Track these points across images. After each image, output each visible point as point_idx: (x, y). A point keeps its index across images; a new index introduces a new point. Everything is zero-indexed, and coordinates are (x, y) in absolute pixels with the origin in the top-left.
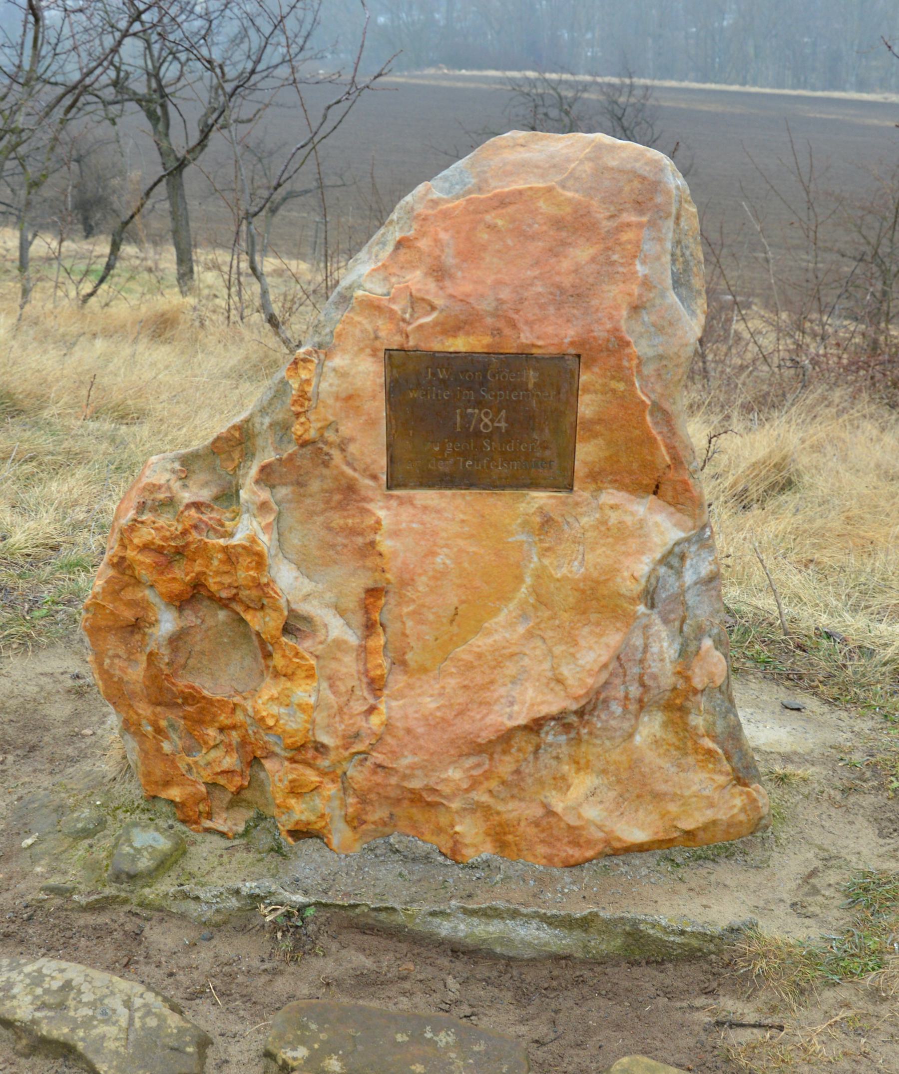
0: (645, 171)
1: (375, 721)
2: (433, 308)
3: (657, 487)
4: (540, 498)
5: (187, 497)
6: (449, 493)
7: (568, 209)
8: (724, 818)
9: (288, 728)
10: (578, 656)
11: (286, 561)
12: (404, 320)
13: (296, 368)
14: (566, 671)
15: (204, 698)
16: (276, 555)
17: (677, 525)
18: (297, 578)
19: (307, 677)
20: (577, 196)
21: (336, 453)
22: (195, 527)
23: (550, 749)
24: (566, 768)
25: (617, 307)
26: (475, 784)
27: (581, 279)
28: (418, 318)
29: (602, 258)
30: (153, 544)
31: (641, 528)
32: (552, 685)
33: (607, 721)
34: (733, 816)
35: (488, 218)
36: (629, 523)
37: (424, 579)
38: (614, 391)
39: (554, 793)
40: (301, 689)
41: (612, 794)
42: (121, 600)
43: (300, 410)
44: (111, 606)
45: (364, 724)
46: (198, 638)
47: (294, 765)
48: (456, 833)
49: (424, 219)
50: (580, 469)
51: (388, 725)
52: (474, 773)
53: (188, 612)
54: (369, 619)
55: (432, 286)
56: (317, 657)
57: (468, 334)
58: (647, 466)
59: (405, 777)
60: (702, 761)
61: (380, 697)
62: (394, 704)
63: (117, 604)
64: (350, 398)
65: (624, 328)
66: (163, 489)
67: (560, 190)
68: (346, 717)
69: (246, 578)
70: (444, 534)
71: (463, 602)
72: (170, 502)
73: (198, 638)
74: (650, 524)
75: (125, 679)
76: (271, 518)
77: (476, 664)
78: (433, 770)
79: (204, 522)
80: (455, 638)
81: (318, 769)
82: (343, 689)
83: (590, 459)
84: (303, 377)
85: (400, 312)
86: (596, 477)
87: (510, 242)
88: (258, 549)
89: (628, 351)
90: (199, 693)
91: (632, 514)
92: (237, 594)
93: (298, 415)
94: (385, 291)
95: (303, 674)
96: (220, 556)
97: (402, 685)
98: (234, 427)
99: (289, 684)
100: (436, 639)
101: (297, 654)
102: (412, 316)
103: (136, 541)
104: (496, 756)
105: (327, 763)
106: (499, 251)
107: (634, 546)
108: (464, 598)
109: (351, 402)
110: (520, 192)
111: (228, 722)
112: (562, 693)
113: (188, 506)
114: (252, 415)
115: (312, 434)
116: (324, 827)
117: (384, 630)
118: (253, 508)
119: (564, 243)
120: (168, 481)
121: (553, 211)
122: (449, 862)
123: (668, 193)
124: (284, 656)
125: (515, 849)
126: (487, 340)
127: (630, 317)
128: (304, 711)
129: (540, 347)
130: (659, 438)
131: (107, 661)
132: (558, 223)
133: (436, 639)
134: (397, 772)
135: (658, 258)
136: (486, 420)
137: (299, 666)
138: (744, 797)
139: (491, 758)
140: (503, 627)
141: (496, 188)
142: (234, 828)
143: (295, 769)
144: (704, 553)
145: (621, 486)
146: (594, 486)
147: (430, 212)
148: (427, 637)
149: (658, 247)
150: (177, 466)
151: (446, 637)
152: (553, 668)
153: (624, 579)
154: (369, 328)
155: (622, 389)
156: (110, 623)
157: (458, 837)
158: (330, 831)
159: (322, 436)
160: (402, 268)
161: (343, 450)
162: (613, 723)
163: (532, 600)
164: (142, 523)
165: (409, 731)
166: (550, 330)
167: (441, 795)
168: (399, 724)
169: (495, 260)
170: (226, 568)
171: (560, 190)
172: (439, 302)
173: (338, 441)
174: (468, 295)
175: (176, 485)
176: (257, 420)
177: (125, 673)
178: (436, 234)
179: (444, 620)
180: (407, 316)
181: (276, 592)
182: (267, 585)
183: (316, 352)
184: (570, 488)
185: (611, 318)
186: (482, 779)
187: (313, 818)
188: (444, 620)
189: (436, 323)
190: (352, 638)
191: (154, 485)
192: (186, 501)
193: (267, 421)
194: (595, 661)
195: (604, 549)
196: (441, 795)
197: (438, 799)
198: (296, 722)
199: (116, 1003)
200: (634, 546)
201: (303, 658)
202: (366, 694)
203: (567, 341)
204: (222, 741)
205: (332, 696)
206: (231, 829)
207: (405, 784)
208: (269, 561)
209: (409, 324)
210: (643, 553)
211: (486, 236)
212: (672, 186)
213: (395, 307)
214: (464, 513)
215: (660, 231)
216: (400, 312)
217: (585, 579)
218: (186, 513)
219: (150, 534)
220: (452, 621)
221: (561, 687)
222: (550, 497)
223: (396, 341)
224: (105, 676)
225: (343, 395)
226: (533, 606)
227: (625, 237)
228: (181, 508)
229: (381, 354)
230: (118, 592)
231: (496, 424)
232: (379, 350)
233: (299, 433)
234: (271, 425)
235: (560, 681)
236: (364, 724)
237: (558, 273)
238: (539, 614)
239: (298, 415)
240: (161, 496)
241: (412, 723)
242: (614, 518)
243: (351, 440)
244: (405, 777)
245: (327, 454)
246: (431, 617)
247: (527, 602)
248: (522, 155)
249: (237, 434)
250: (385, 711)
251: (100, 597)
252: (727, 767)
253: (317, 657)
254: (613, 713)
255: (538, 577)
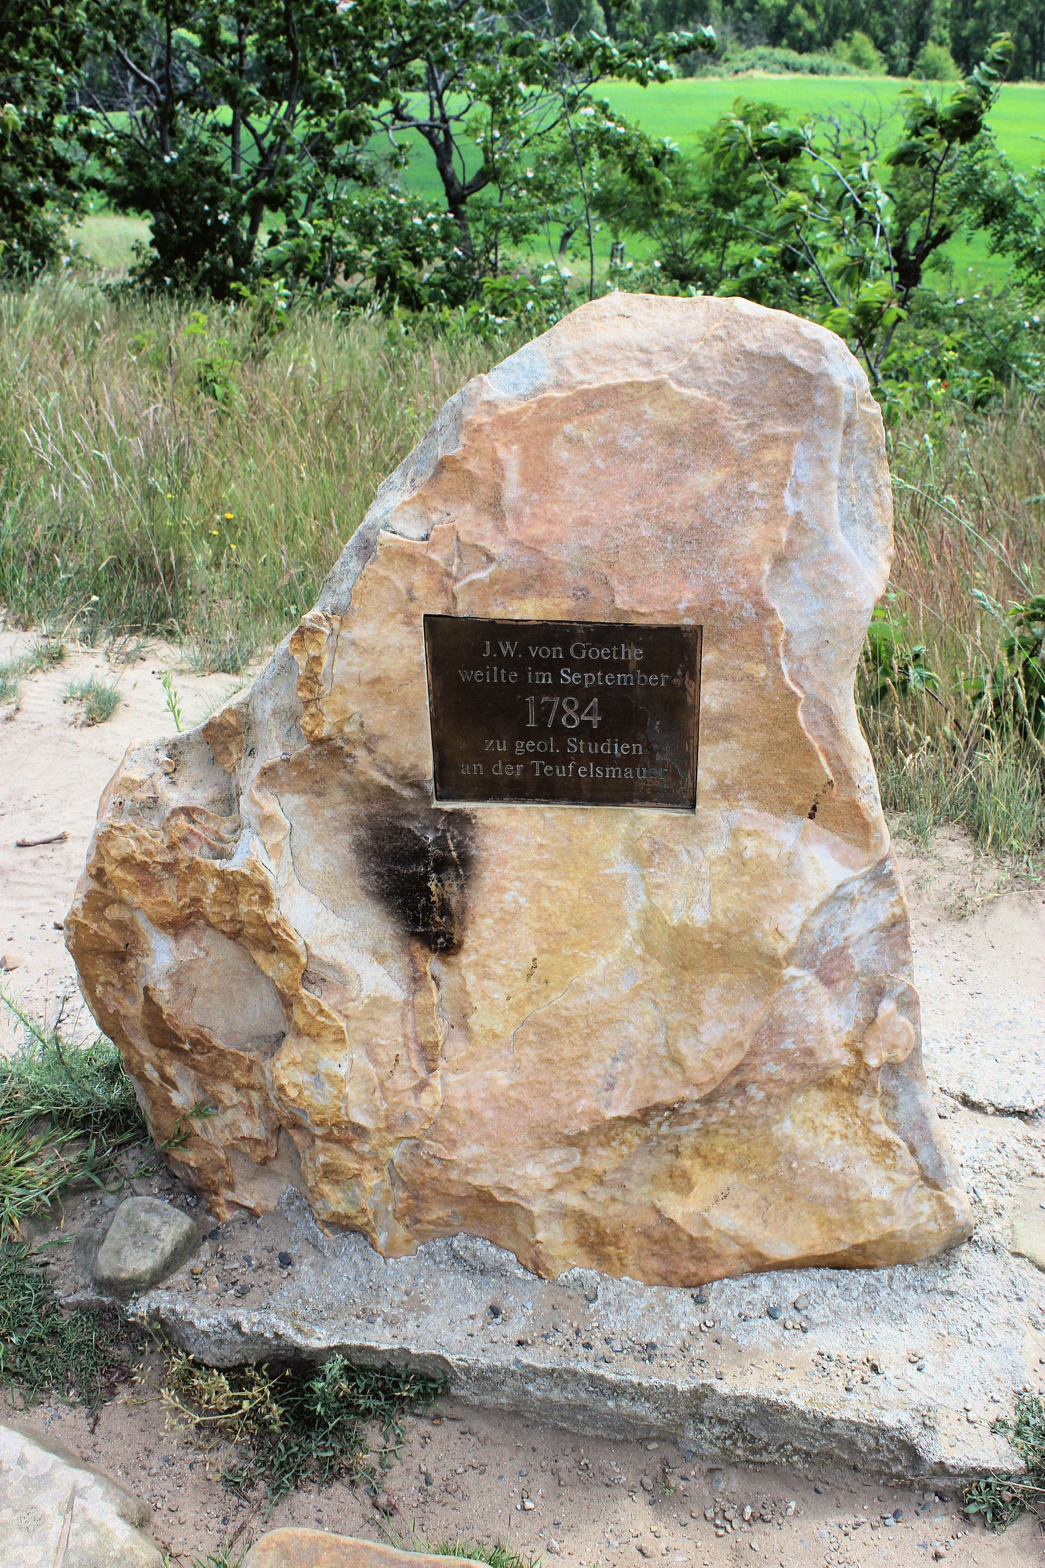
0: (799, 357)
1: (426, 1099)
2: (490, 559)
3: (814, 808)
4: (651, 816)
5: (174, 797)
6: (520, 807)
7: (686, 415)
8: (906, 1228)
9: (315, 1103)
10: (701, 1029)
11: (304, 891)
12: (449, 575)
13: (302, 640)
14: (685, 1048)
15: (214, 1047)
16: (289, 884)
17: (845, 861)
18: (318, 915)
19: (336, 1041)
20: (699, 394)
21: (360, 753)
22: (185, 840)
23: (665, 1142)
24: (688, 1163)
25: (757, 560)
26: (563, 1182)
27: (702, 517)
28: (469, 573)
29: (732, 488)
30: (134, 858)
31: (791, 864)
32: (667, 1064)
33: (744, 1108)
34: (918, 1226)
35: (569, 428)
36: (774, 857)
37: (489, 921)
38: (751, 677)
39: (671, 1194)
40: (328, 1055)
41: (753, 1197)
42: (106, 920)
43: (309, 696)
44: (94, 926)
45: (412, 1103)
46: (205, 972)
47: (328, 1145)
48: (538, 1242)
49: (475, 431)
50: (705, 780)
51: (446, 1108)
52: (560, 1169)
53: (186, 940)
54: (416, 970)
55: (487, 526)
56: (346, 1017)
57: (541, 595)
58: (800, 781)
59: (467, 1171)
60: (878, 1155)
61: (434, 1070)
62: (452, 1078)
63: (102, 924)
64: (377, 680)
65: (765, 590)
66: (145, 787)
67: (674, 386)
68: (389, 1094)
69: (248, 913)
70: (515, 863)
71: (542, 951)
72: (153, 803)
73: (205, 972)
74: (803, 860)
75: (122, 1012)
76: (277, 837)
77: (563, 1031)
78: (506, 1165)
79: (195, 834)
80: (534, 997)
81: (356, 1153)
82: (383, 1057)
83: (718, 768)
84: (312, 653)
85: (442, 564)
86: (725, 791)
87: (599, 463)
88: (262, 878)
89: (770, 622)
90: (209, 1042)
91: (780, 845)
92: (241, 930)
93: (307, 703)
94: (423, 534)
95: (332, 1037)
96: (216, 881)
97: (463, 1054)
98: (229, 710)
99: (314, 1047)
100: (508, 998)
101: (321, 1011)
102: (459, 569)
103: (113, 852)
104: (590, 1150)
105: (366, 1148)
106: (584, 476)
107: (779, 889)
108: (545, 946)
109: (378, 687)
110: (614, 390)
111: (243, 1081)
112: (679, 1076)
113: (175, 813)
114: (252, 695)
115: (324, 731)
116: (367, 1224)
117: (438, 985)
118: (254, 822)
119: (681, 466)
120: (151, 776)
121: (667, 418)
122: (530, 1277)
123: (833, 390)
124: (305, 1012)
125: (618, 1264)
126: (568, 604)
127: (774, 573)
128: (333, 1084)
129: (643, 614)
130: (816, 745)
131: (99, 989)
132: (670, 436)
133: (508, 998)
134: (458, 1165)
135: (820, 487)
136: (570, 712)
137: (325, 1027)
138: (934, 1202)
139: (584, 1153)
140: (600, 984)
141: (582, 382)
142: (263, 1203)
143: (328, 1150)
144: (883, 893)
145: (764, 803)
146: (726, 804)
147: (486, 419)
148: (496, 996)
149: (819, 473)
150: (163, 756)
151: (522, 996)
152: (667, 1044)
153: (765, 933)
154: (401, 585)
155: (762, 675)
156: (96, 946)
157: (541, 1247)
158: (373, 1229)
159: (341, 731)
160: (446, 501)
161: (371, 751)
162: (752, 1109)
163: (639, 951)
164: (120, 829)
165: (472, 1114)
166: (658, 591)
167: (515, 1195)
168: (458, 1105)
169: (579, 490)
170: (225, 897)
171: (674, 386)
172: (497, 550)
173: (364, 738)
174: (541, 541)
175: (162, 782)
176: (257, 702)
177: (121, 1004)
178: (494, 451)
179: (519, 975)
180: (454, 569)
181: (288, 935)
182: (277, 925)
183: (328, 619)
184: (692, 806)
185: (746, 574)
186: (572, 1177)
187: (352, 1212)
188: (519, 975)
189: (493, 581)
190: (397, 993)
191: (133, 781)
192: (174, 805)
193: (269, 706)
194: (724, 1038)
195: (737, 890)
196: (515, 1195)
197: (514, 1200)
198: (324, 1096)
199: (48, 1504)
200: (779, 889)
201: (328, 1017)
202: (415, 1064)
203: (682, 606)
204: (240, 1102)
205: (371, 1067)
206: (259, 1204)
207: (470, 1179)
208: (276, 894)
209: (456, 580)
210: (792, 900)
211: (565, 455)
212: (840, 380)
213: (434, 556)
214: (544, 836)
215: (819, 447)
216: (442, 564)
217: (713, 927)
218: (173, 822)
219: (129, 845)
220: (529, 976)
221: (678, 1069)
222: (664, 817)
223: (437, 609)
224: (99, 1006)
225: (367, 677)
226: (641, 958)
227: (767, 456)
228: (168, 815)
229: (420, 621)
230: (102, 910)
231: (583, 717)
232: (416, 616)
233: (309, 728)
234: (274, 713)
235: (676, 1061)
236: (412, 1103)
237: (670, 508)
238: (650, 969)
239: (307, 703)
240: (142, 795)
241: (477, 1105)
242: (750, 847)
243: (382, 737)
244: (467, 1171)
245: (349, 755)
246: (500, 971)
247: (632, 953)
248: (629, 332)
249: (233, 721)
250: (440, 1089)
251: (81, 914)
252: (912, 1164)
253: (346, 1017)
254: (752, 1098)
255: (648, 921)
